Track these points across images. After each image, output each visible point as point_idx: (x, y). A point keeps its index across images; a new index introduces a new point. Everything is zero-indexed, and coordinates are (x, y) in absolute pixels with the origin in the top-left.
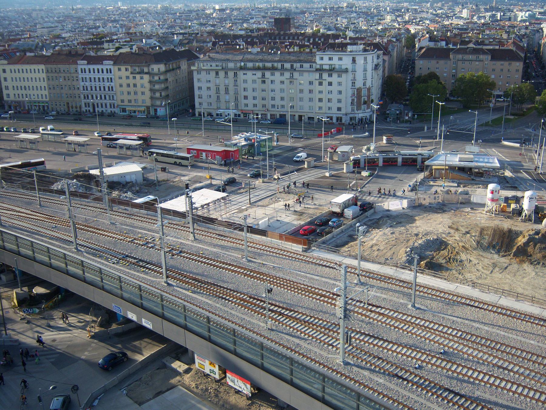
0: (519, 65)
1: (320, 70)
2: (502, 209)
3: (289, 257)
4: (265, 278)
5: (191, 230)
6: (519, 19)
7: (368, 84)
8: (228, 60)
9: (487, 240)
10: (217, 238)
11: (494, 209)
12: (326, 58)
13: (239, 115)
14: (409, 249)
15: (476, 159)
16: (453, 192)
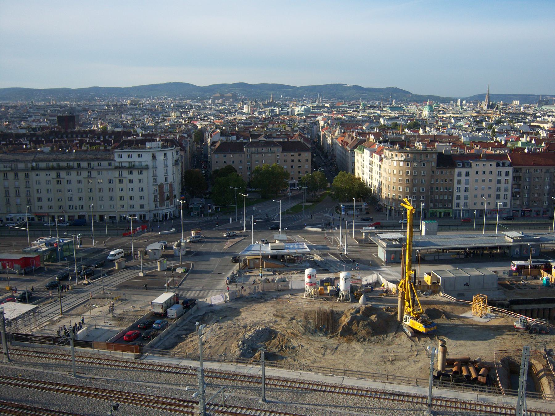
0: (307, 156)
1: (120, 168)
2: (320, 292)
3: (122, 366)
4: (100, 393)
5: (4, 351)
6: (296, 113)
7: (170, 180)
8: (17, 161)
9: (312, 325)
10: (35, 357)
11: (313, 293)
12: (125, 156)
13: (33, 219)
14: (240, 343)
15: (287, 246)
16: (270, 281)
